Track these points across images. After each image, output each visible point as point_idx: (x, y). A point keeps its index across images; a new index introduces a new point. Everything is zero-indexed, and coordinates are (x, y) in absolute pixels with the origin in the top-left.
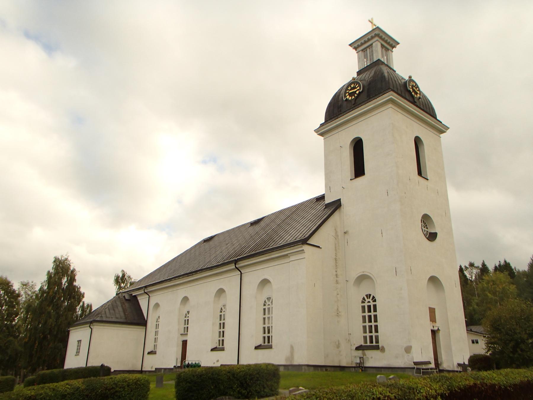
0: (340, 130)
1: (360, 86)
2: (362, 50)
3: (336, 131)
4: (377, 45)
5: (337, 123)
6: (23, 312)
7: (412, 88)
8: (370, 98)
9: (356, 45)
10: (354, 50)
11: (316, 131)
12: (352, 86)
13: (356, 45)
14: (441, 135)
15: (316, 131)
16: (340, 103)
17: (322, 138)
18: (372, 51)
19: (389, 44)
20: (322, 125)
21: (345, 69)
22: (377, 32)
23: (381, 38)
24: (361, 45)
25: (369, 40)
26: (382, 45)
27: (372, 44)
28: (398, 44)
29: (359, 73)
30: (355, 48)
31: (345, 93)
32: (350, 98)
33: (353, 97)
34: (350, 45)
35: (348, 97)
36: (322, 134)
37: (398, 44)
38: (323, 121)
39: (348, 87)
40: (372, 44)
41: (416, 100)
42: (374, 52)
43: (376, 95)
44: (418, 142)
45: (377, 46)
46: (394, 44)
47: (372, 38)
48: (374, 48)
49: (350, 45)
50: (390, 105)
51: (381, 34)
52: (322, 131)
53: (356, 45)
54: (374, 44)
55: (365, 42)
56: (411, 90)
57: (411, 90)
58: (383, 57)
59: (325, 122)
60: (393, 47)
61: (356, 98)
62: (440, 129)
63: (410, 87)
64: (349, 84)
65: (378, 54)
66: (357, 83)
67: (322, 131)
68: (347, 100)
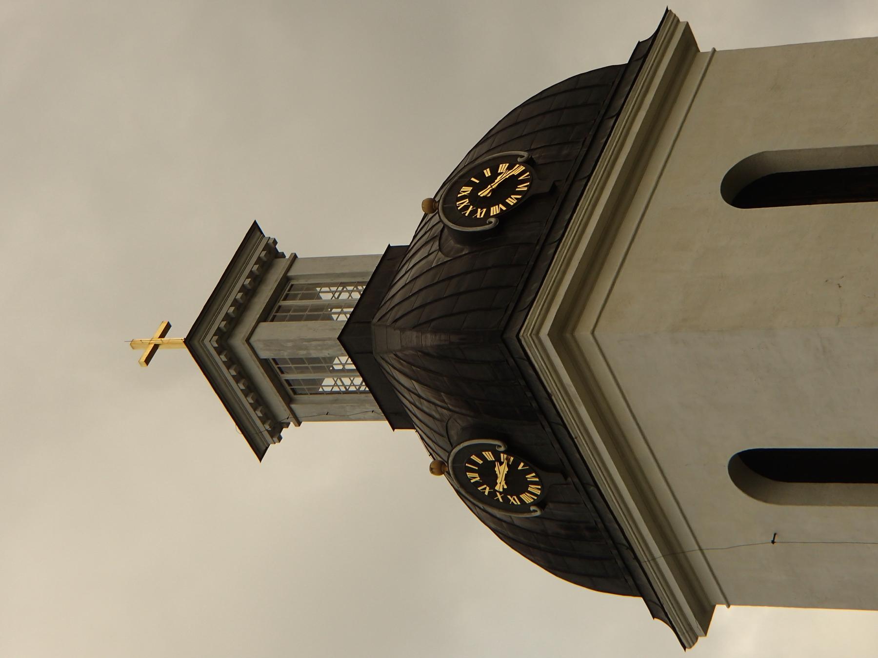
0: (689, 543)
1: (478, 450)
2: (289, 400)
3: (696, 559)
4: (268, 343)
5: (657, 553)
6: (511, 184)
7: (487, 203)
8: (541, 410)
9: (260, 429)
10: (284, 432)
11: (687, 639)
12: (474, 477)
13: (264, 428)
14: (704, 45)
15: (687, 639)
16: (551, 527)
17: (721, 612)
18: (294, 361)
19: (258, 277)
20: (657, 610)
21: (363, 467)
22: (210, 343)
23: (233, 322)
24: (261, 406)
25: (243, 375)
26: (266, 316)
27: (265, 364)
28: (255, 227)
29: (398, 419)
30: (276, 433)
31: (506, 506)
32: (535, 489)
33: (530, 477)
34: (260, 453)
35: (527, 498)
36: (705, 616)
37: (255, 227)
38: (637, 605)
39: (480, 497)
40: (265, 364)
41: (546, 188)
42: (302, 353)
43: (529, 386)
44: (756, 186)
45: (274, 338)
46: (259, 252)
47: (234, 360)
48: (285, 354)
49: (260, 453)
50: (583, 333)
51: (219, 322)
52: (688, 608)
53: (260, 429)
54: (264, 355)
55: (252, 388)
56: (495, 210)
57: (495, 210)
58: (321, 313)
59: (641, 594)
60: (272, 252)
61: (535, 464)
62: (672, 51)
63: (480, 214)
64: (468, 492)
65: (310, 338)
66: (463, 457)
67: (688, 608)
68: (540, 503)
